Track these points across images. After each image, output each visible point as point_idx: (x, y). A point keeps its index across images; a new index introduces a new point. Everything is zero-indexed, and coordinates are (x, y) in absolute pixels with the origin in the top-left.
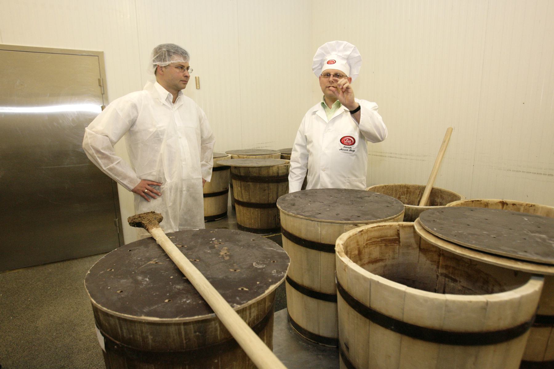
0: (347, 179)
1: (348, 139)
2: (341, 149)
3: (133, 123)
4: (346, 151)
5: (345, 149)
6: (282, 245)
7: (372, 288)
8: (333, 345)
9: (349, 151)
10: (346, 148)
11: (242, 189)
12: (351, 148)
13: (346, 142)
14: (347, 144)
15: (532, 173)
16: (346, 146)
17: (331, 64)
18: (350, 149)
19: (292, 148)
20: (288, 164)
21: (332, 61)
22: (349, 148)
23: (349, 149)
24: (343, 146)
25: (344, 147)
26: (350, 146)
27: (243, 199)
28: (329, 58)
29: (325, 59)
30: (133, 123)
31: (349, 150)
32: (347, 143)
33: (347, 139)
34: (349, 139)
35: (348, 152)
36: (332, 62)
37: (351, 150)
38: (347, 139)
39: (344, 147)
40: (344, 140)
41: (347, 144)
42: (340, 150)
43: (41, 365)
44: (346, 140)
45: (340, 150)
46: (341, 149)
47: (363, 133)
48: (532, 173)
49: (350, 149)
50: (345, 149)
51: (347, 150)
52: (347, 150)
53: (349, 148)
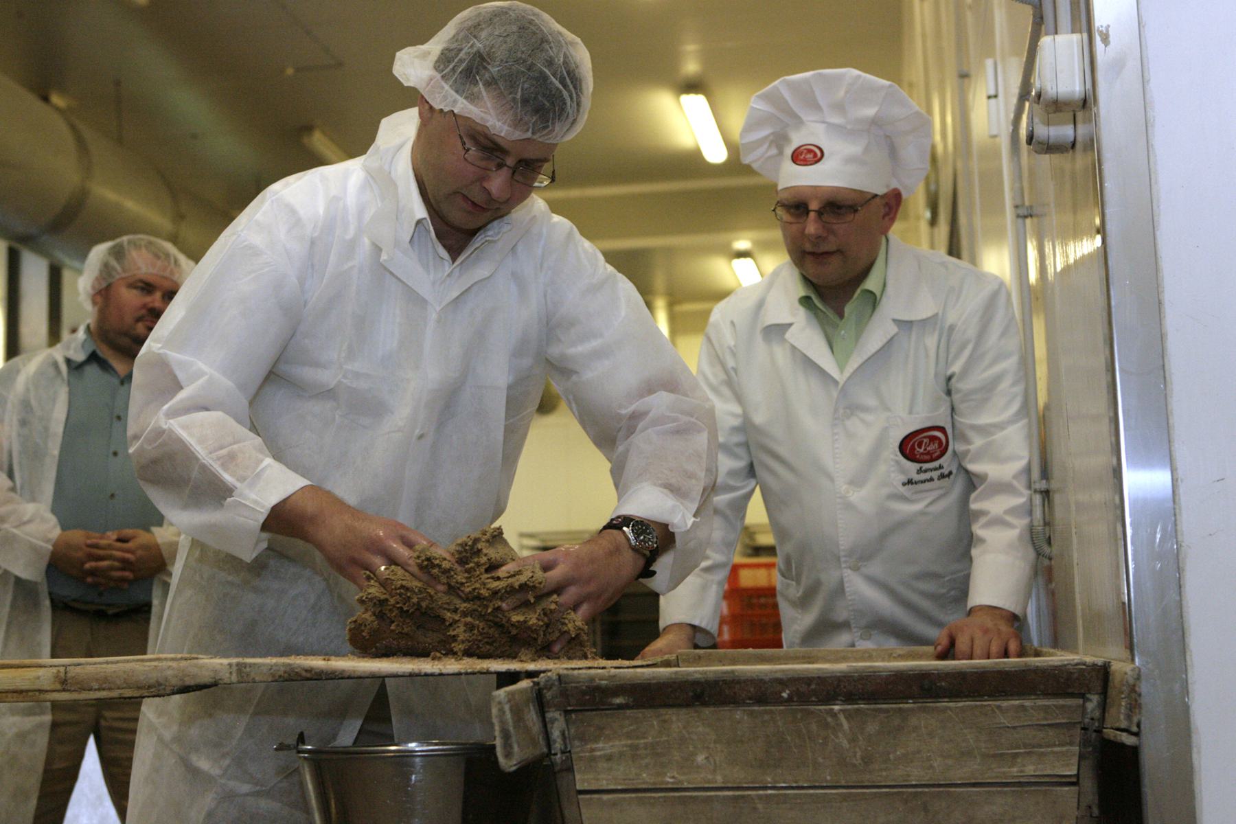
0: (947, 579)
1: (805, 149)
2: (910, 482)
4: (928, 485)
5: (923, 476)
7: (975, 647)
8: (791, 794)
10: (926, 471)
12: (941, 467)
13: (922, 450)
14: (927, 457)
16: (926, 466)
17: (805, 163)
18: (938, 473)
19: (650, 411)
20: (809, 738)
21: (810, 151)
22: (936, 469)
23: (935, 474)
24: (912, 467)
25: (920, 471)
26: (936, 464)
28: (798, 139)
29: (848, 309)
31: (935, 477)
32: (928, 453)
33: (925, 440)
34: (933, 439)
35: (936, 483)
36: (810, 156)
37: (942, 476)
38: (925, 440)
39: (920, 471)
40: (913, 445)
41: (927, 457)
44: (920, 445)
46: (910, 482)
49: (938, 473)
50: (923, 476)
51: (931, 480)
52: (931, 480)
53: (936, 469)
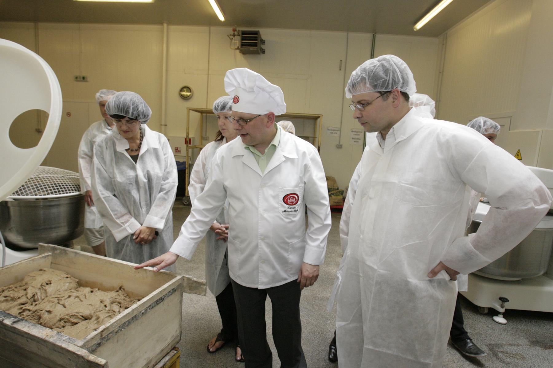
2: (285, 211)
3: (319, 117)
5: (289, 210)
6: (268, 163)
9: (293, 212)
10: (290, 208)
11: (213, 348)
12: (295, 208)
13: (290, 201)
14: (291, 204)
15: (134, 149)
23: (293, 210)
25: (289, 208)
27: (212, 205)
30: (319, 117)
31: (293, 211)
32: (292, 202)
34: (294, 197)
42: (283, 212)
43: (102, 305)
45: (283, 212)
46: (285, 211)
47: (328, 178)
48: (134, 149)
50: (289, 210)
51: (292, 211)
52: (292, 211)
